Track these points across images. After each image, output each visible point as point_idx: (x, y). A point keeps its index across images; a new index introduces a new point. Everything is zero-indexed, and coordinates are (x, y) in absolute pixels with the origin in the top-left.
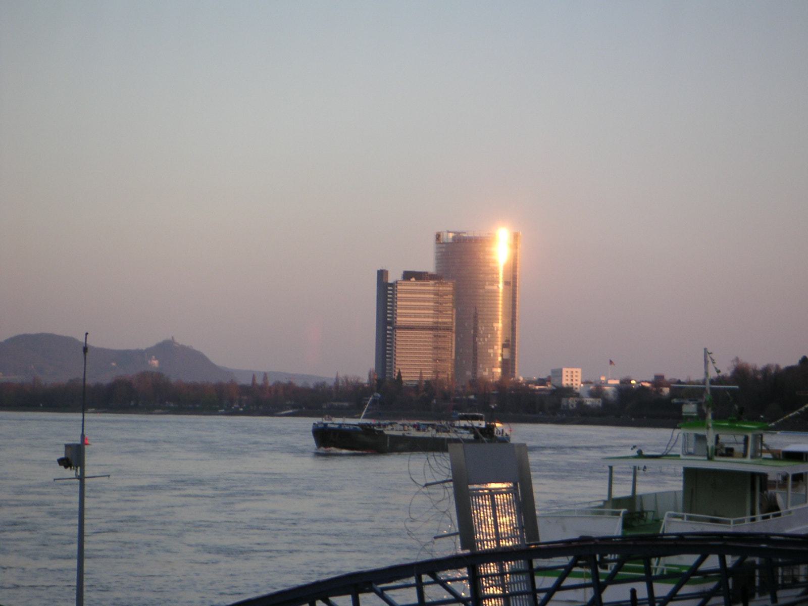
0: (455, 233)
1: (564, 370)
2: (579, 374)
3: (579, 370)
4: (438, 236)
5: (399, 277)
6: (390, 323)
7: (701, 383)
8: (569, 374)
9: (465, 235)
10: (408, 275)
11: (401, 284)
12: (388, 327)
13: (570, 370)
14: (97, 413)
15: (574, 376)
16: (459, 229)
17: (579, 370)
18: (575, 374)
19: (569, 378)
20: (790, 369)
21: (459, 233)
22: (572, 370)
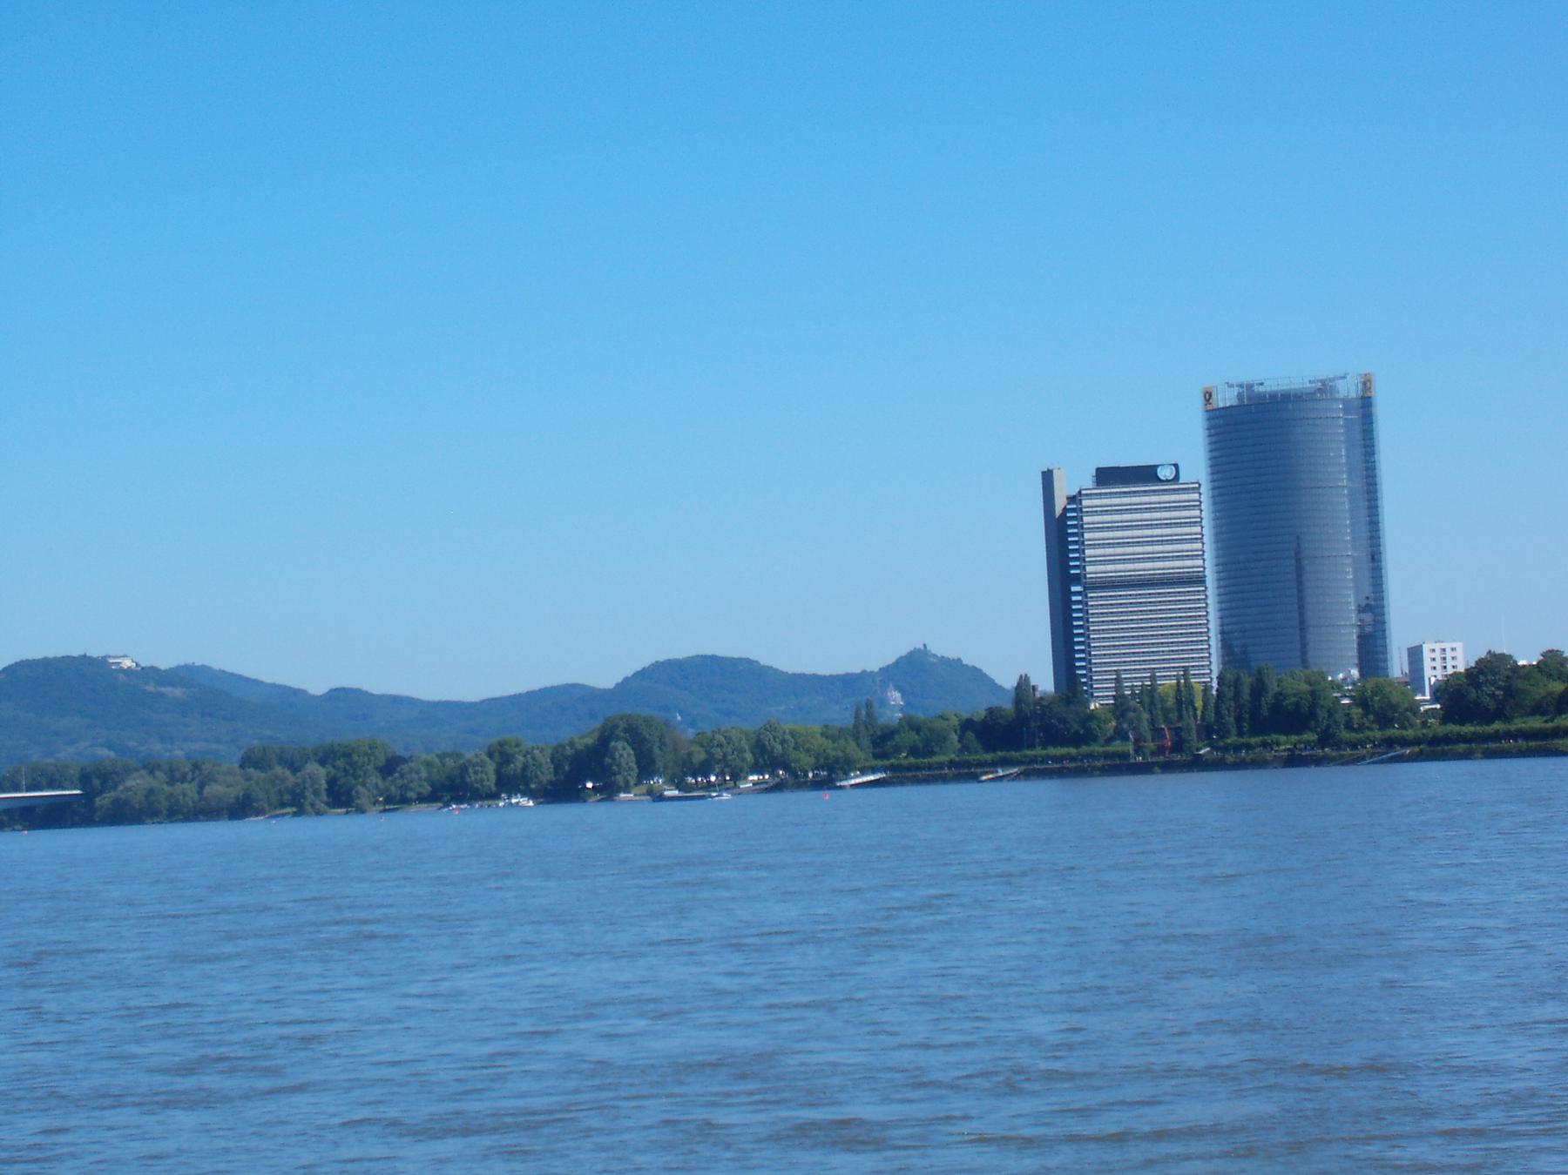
0: (1241, 386)
1: (1426, 649)
2: (1459, 653)
3: (1458, 645)
4: (1208, 396)
5: (1087, 481)
6: (1077, 579)
7: (547, 775)
8: (1437, 655)
9: (1261, 389)
10: (1107, 476)
11: (1089, 496)
12: (1074, 589)
13: (1438, 647)
14: (902, 783)
15: (1439, 660)
16: (1246, 378)
17: (1458, 645)
18: (1449, 654)
19: (1438, 664)
20: (605, 692)
21: (1250, 386)
22: (1443, 645)
